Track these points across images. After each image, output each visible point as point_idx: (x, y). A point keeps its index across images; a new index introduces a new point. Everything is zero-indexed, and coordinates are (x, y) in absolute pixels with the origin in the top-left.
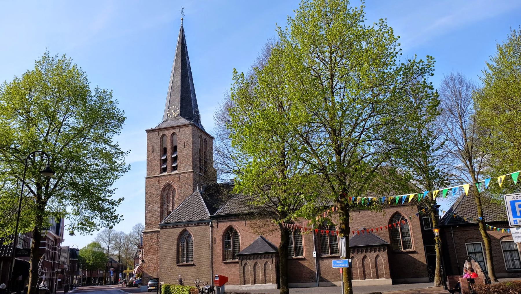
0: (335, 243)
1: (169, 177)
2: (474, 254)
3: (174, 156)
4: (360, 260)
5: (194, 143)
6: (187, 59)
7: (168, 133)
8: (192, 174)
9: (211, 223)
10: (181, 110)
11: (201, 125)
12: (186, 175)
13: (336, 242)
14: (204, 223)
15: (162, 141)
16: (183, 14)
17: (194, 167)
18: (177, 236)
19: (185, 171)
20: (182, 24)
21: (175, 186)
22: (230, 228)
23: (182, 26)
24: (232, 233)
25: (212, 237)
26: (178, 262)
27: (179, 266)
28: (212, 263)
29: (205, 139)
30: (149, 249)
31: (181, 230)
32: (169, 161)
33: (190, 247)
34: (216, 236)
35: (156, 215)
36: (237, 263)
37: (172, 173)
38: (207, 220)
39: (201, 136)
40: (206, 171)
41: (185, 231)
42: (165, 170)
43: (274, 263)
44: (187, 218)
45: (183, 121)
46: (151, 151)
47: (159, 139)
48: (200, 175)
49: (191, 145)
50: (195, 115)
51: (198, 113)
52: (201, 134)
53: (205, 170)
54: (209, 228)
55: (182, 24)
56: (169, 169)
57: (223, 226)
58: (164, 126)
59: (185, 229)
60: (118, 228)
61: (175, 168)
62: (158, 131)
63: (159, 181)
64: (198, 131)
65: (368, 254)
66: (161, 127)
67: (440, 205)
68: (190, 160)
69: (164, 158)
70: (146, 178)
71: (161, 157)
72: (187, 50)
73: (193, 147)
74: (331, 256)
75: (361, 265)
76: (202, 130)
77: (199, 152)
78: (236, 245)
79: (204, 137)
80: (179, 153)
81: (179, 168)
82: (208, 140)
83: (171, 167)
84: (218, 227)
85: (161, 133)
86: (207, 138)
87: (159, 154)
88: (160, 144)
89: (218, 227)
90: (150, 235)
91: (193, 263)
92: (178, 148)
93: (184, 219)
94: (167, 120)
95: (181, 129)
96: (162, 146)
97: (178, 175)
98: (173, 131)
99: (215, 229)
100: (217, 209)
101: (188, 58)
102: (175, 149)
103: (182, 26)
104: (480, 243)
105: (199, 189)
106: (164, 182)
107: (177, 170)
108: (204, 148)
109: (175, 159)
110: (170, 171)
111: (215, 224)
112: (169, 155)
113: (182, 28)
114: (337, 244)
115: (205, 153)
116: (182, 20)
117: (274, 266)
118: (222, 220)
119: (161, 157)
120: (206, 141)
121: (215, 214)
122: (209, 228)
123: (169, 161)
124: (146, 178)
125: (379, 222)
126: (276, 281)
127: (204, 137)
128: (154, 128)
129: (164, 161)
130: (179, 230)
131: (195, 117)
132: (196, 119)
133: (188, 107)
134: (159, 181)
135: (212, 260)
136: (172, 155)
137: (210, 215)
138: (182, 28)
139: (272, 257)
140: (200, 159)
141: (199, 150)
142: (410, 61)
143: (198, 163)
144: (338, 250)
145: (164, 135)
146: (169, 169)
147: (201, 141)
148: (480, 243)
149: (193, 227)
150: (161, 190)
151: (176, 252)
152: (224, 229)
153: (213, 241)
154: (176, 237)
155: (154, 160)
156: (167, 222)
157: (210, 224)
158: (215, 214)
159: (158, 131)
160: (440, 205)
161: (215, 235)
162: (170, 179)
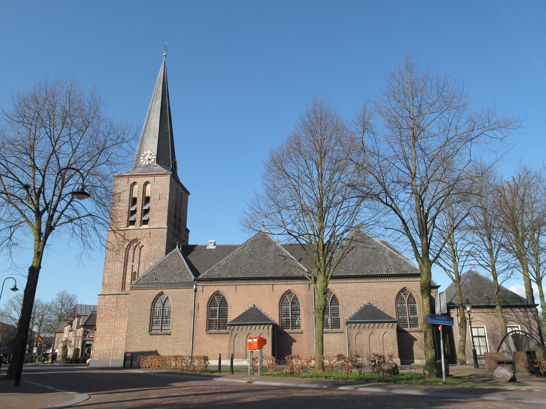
0: (337, 317)
1: (136, 231)
2: (477, 338)
8: (166, 229)
9: (195, 286)
13: (338, 316)
19: (158, 227)
21: (143, 242)
22: (217, 294)
26: (150, 330)
27: (151, 335)
29: (181, 193)
31: (158, 291)
34: (199, 302)
37: (128, 228)
38: (191, 282)
39: (178, 189)
40: (179, 229)
41: (161, 294)
42: (133, 223)
44: (165, 279)
45: (159, 169)
48: (174, 233)
52: (178, 186)
54: (192, 291)
56: (138, 222)
57: (210, 290)
61: (146, 222)
62: (128, 178)
64: (176, 182)
67: (440, 286)
78: (224, 313)
79: (181, 190)
81: (150, 222)
82: (184, 195)
83: (141, 221)
85: (132, 180)
86: (184, 192)
87: (127, 204)
98: (146, 179)
102: (147, 200)
104: (484, 327)
105: (179, 248)
107: (134, 225)
108: (179, 203)
110: (139, 225)
111: (199, 288)
112: (139, 206)
114: (339, 318)
115: (180, 208)
118: (208, 284)
120: (182, 196)
121: (200, 277)
122: (192, 291)
123: (139, 213)
125: (385, 297)
127: (181, 190)
140: (175, 215)
143: (173, 219)
144: (340, 325)
145: (135, 183)
146: (138, 222)
148: (484, 327)
152: (211, 294)
153: (196, 307)
154: (277, 302)
156: (140, 282)
159: (128, 178)
160: (440, 286)
161: (199, 301)
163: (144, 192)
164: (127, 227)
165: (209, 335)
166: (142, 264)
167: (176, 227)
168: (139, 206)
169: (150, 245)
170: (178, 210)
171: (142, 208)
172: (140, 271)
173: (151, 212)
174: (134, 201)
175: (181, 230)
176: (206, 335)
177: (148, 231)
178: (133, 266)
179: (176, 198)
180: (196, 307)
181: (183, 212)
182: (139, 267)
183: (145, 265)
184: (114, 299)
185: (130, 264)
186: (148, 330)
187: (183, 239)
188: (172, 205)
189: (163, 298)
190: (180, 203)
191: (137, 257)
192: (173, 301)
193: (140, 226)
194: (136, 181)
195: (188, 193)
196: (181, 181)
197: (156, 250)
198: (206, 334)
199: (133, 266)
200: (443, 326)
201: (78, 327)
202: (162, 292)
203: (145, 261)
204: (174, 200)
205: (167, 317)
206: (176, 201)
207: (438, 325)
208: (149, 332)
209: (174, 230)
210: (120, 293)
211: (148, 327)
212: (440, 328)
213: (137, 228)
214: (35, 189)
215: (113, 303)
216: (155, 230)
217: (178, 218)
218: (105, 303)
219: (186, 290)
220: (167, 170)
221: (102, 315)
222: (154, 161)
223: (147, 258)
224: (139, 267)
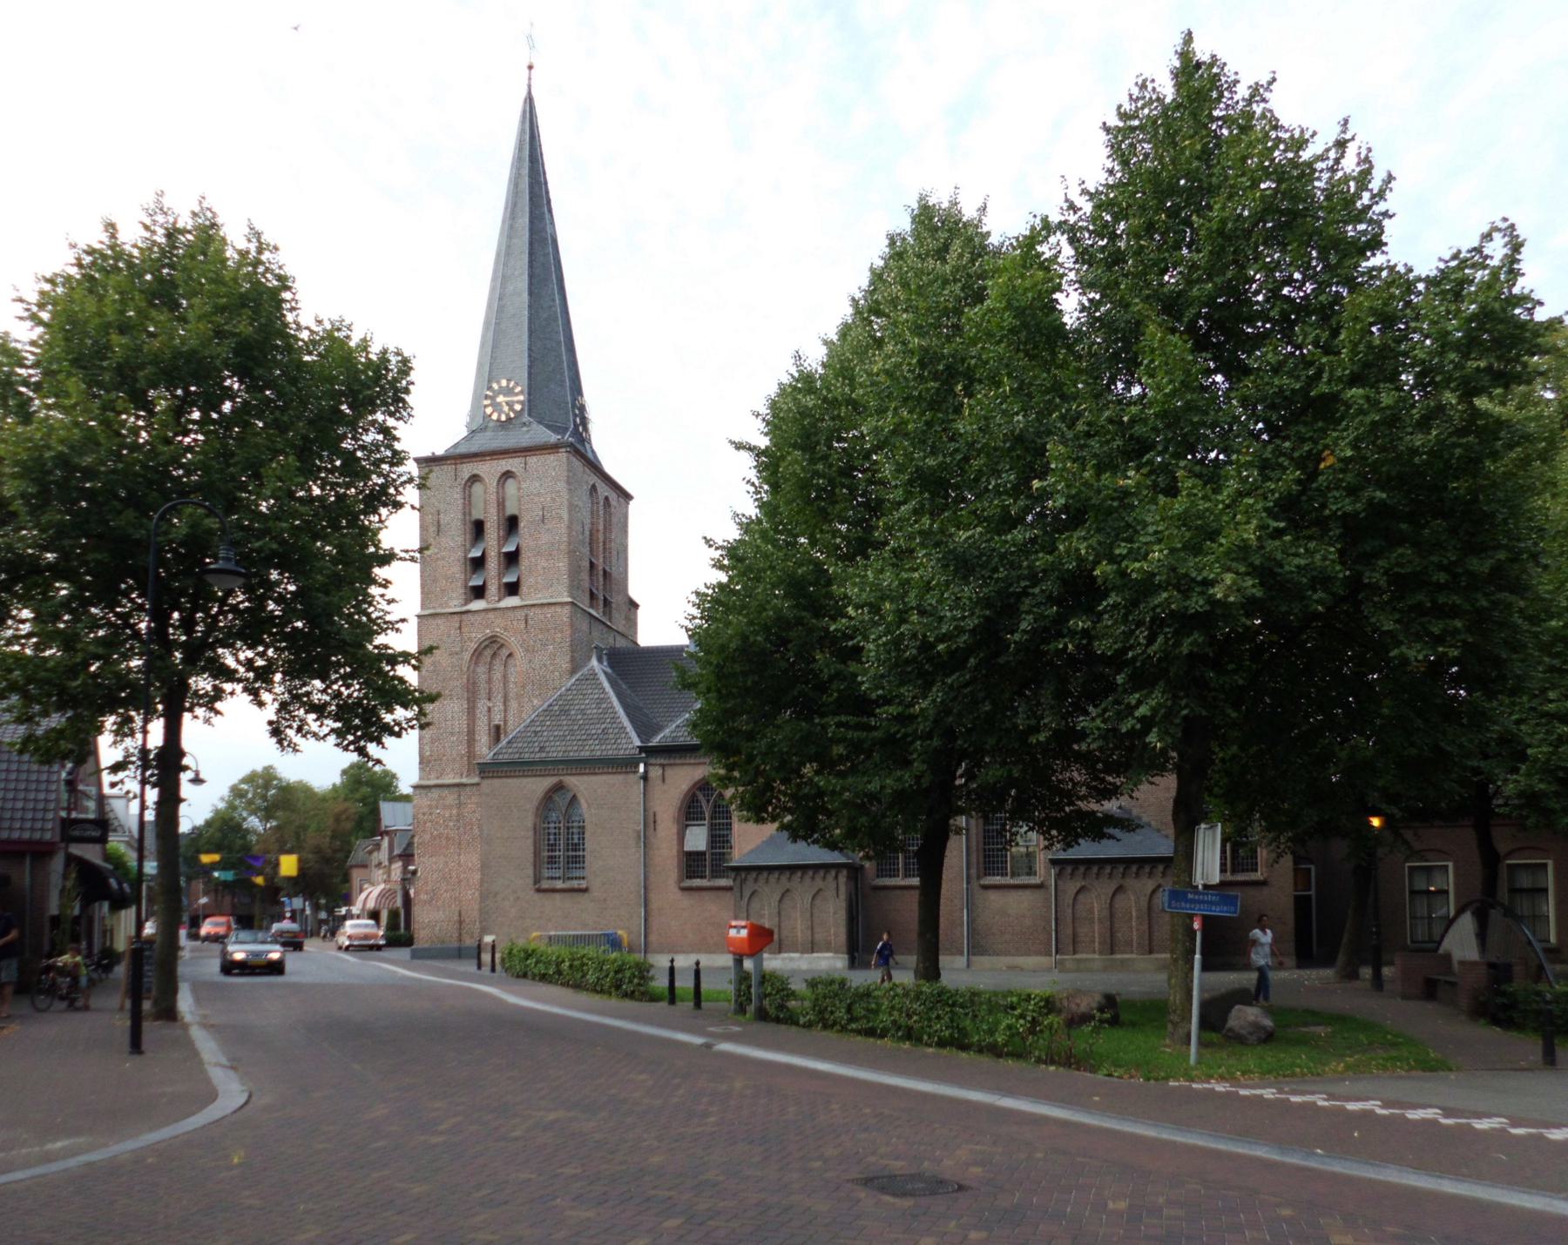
1: (491, 615)
3: (510, 548)
4: (1103, 897)
5: (572, 508)
6: (547, 216)
7: (489, 470)
10: (529, 394)
11: (593, 451)
12: (549, 611)
14: (625, 765)
15: (470, 496)
16: (532, 47)
17: (573, 587)
18: (535, 803)
19: (545, 601)
20: (529, 86)
23: (529, 93)
24: (708, 801)
25: (645, 810)
27: (539, 890)
28: (646, 888)
29: (606, 498)
30: (434, 838)
31: (548, 782)
32: (492, 564)
33: (576, 837)
35: (452, 734)
36: (729, 889)
39: (594, 487)
40: (607, 603)
41: (559, 788)
42: (479, 592)
43: (843, 896)
46: (432, 529)
47: (459, 489)
48: (590, 614)
49: (566, 516)
50: (575, 415)
51: (582, 408)
52: (594, 479)
53: (605, 599)
55: (529, 86)
58: (474, 449)
59: (561, 782)
60: (404, 787)
61: (513, 589)
63: (460, 628)
65: (1130, 882)
66: (463, 450)
68: (563, 565)
69: (476, 553)
70: (419, 616)
71: (467, 551)
72: (546, 183)
73: (571, 522)
74: (1012, 882)
75: (1106, 913)
76: (595, 466)
77: (587, 540)
79: (604, 490)
80: (526, 538)
81: (524, 589)
82: (613, 503)
84: (664, 780)
86: (613, 496)
87: (460, 540)
88: (460, 507)
89: (664, 780)
90: (435, 794)
91: (583, 884)
92: (522, 525)
93: (556, 752)
94: (482, 429)
95: (533, 460)
96: (470, 514)
97: (522, 613)
99: (657, 789)
100: (660, 728)
101: (550, 211)
102: (512, 524)
103: (529, 93)
106: (477, 635)
108: (601, 527)
109: (512, 559)
111: (655, 772)
112: (492, 543)
113: (530, 100)
115: (604, 543)
116: (530, 67)
117: (841, 904)
119: (467, 551)
123: (492, 564)
124: (419, 616)
126: (845, 949)
128: (440, 452)
129: (478, 564)
130: (541, 785)
131: (575, 421)
132: (576, 426)
133: (552, 386)
134: (460, 628)
135: (646, 879)
136: (500, 546)
137: (639, 744)
138: (530, 100)
139: (836, 877)
140: (592, 565)
141: (587, 533)
142: (1411, 270)
143: (585, 576)
145: (475, 478)
146: (492, 589)
147: (594, 503)
149: (585, 778)
150: (467, 656)
151: (532, 848)
153: (650, 822)
154: (531, 807)
155: (443, 558)
157: (642, 768)
158: (656, 741)
162: (498, 626)
163: (501, 504)
164: (466, 604)
165: (686, 893)
166: (513, 704)
167: (597, 599)
168: (492, 543)
169: (527, 651)
170: (601, 548)
171: (500, 549)
172: (510, 722)
173: (525, 560)
174: (478, 528)
175: (614, 606)
176: (679, 894)
177: (521, 614)
178: (489, 710)
179: (592, 513)
180: (650, 822)
181: (614, 553)
182: (505, 711)
183: (521, 706)
184: (451, 798)
185: (482, 705)
186: (531, 881)
187: (621, 629)
188: (581, 537)
189: (561, 801)
190: (605, 528)
191: (497, 685)
192: (589, 805)
193: (499, 600)
194: (475, 472)
195: (627, 497)
196: (609, 468)
197: (545, 665)
198: (676, 890)
199: (489, 710)
200: (1206, 920)
201: (391, 860)
202: (561, 782)
203: (519, 697)
204: (587, 521)
205: (576, 847)
206: (592, 524)
207: (1191, 917)
208: (535, 883)
209: (591, 606)
210: (464, 780)
211: (530, 872)
212: (1196, 926)
213: (491, 606)
214: (1333, 170)
215: (450, 807)
216: (538, 611)
217: (601, 573)
218: (430, 807)
219: (621, 777)
220: (558, 433)
221: (427, 837)
222: (522, 409)
223: (523, 687)
224: (505, 711)
